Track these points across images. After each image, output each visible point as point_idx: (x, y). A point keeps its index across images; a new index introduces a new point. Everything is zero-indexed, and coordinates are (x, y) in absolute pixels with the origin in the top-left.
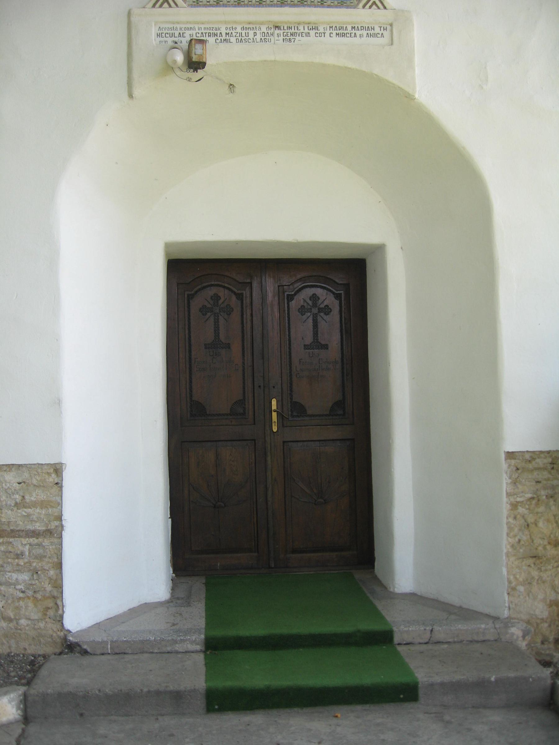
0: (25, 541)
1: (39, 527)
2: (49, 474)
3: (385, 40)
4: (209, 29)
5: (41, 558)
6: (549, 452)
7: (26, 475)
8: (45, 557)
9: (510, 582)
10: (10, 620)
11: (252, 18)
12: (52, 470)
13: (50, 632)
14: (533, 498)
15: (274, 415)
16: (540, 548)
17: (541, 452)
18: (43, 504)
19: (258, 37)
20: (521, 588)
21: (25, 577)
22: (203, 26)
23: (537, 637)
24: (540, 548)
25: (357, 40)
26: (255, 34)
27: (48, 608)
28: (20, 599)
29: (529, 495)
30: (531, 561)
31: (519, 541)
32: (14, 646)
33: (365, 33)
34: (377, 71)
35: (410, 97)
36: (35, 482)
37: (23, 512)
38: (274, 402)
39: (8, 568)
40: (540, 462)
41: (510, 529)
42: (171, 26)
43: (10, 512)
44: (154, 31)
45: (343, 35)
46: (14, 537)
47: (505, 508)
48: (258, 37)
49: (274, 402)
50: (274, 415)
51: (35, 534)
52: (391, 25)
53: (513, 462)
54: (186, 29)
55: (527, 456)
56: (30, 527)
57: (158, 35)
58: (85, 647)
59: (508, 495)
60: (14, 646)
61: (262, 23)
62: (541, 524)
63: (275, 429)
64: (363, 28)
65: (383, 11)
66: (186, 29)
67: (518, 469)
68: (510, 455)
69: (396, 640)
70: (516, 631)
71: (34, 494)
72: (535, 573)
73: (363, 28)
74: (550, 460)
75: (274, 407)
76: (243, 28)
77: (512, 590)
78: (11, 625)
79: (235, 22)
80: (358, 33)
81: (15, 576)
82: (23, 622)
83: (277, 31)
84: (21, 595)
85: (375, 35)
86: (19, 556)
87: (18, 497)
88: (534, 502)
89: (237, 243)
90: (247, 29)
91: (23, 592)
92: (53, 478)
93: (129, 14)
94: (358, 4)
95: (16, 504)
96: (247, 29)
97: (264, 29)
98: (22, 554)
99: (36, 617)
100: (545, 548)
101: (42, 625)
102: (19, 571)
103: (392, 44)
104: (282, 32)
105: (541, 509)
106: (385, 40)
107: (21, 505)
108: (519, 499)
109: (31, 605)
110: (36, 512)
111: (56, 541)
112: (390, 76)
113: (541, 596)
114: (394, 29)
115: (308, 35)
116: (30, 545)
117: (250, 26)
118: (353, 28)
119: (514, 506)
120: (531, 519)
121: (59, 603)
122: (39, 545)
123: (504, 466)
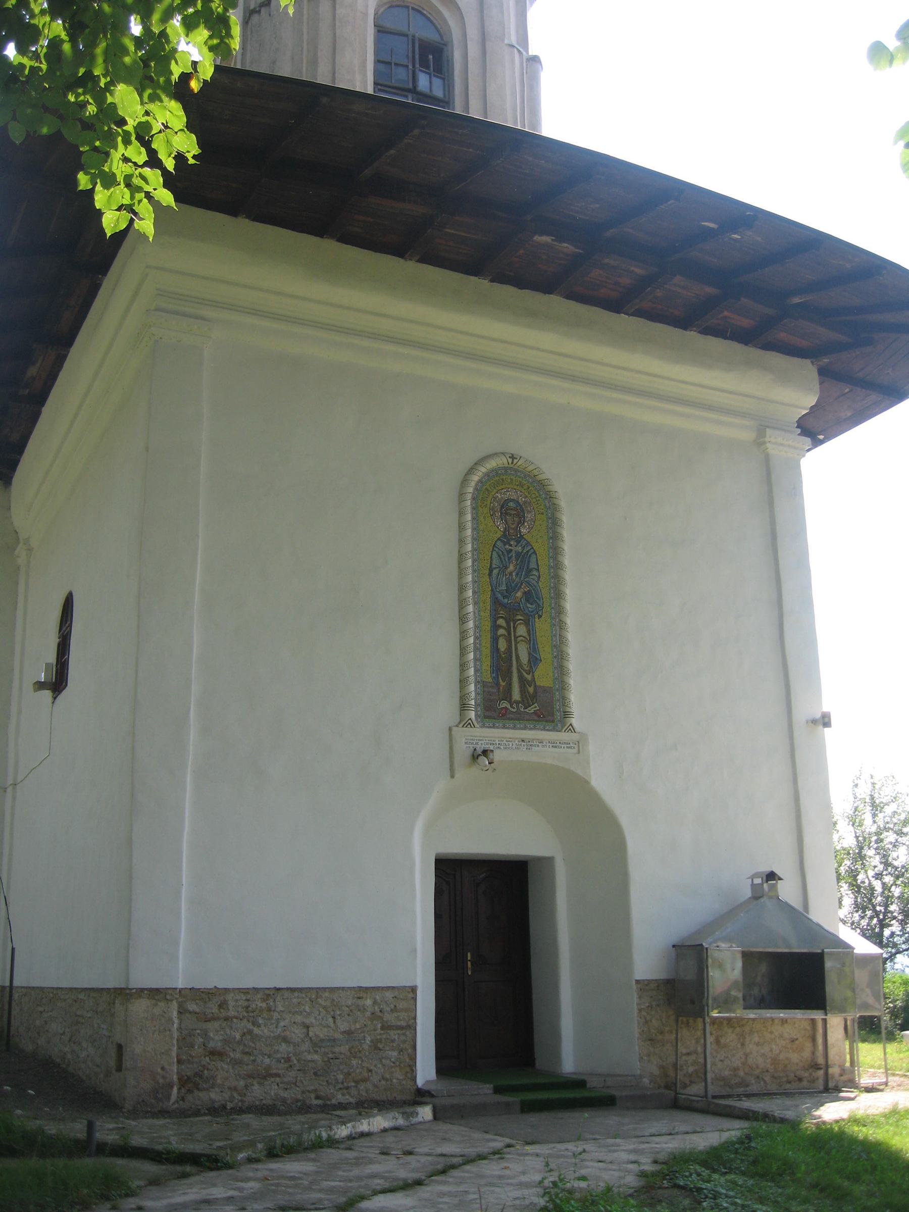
0: (396, 1032)
1: (403, 1023)
2: (409, 992)
3: (575, 751)
4: (490, 740)
5: (404, 1042)
6: (656, 980)
7: (396, 993)
8: (406, 1041)
9: (640, 1054)
10: (387, 1080)
11: (511, 736)
12: (410, 990)
13: (409, 1086)
14: (648, 1006)
15: (469, 963)
16: (654, 1035)
17: (653, 980)
18: (406, 1010)
19: (514, 747)
20: (645, 1058)
21: (395, 1054)
22: (487, 739)
23: (486, 1196)
24: (654, 1035)
25: (562, 750)
26: (513, 745)
27: (407, 1072)
28: (392, 1067)
29: (647, 1005)
30: (649, 1042)
31: (643, 1031)
32: (389, 1095)
33: (565, 746)
34: (572, 768)
35: (587, 782)
36: (401, 997)
37: (395, 1014)
38: (469, 954)
39: (388, 1049)
40: (652, 986)
41: (639, 1023)
42: (472, 738)
43: (388, 1015)
44: (464, 740)
45: (556, 747)
46: (390, 1030)
47: (636, 1011)
48: (514, 747)
49: (469, 954)
50: (469, 963)
51: (401, 1028)
52: (578, 742)
53: (639, 986)
54: (479, 740)
55: (646, 982)
56: (399, 1024)
57: (466, 743)
58: (433, 1093)
59: (638, 1004)
60: (389, 1095)
61: (517, 739)
62: (654, 1021)
63: (470, 973)
64: (565, 743)
65: (574, 734)
66: (479, 740)
67: (641, 990)
68: (638, 982)
69: (588, 1086)
70: (646, 1081)
71: (401, 1004)
72: (652, 1049)
73: (565, 743)
74: (657, 985)
75: (469, 958)
76: (507, 741)
77: (641, 1059)
78: (389, 1083)
79: (503, 738)
80: (563, 746)
81: (390, 1053)
82: (394, 1081)
83: (523, 743)
84: (393, 1065)
85: (570, 747)
86: (393, 1041)
87: (392, 1006)
88: (650, 1008)
89: (456, 854)
90: (509, 741)
91: (394, 1063)
92: (411, 995)
93: (450, 729)
94: (562, 729)
95: (392, 1010)
96: (509, 741)
97: (516, 742)
98: (395, 1040)
99: (401, 1078)
100: (656, 1035)
101: (404, 1082)
102: (393, 1050)
103: (579, 753)
104: (525, 744)
105: (653, 1012)
106: (575, 751)
107: (394, 1010)
108: (642, 1007)
109: (398, 1069)
110: (402, 1015)
111: (413, 1032)
112: (579, 772)
113: (655, 1063)
114: (580, 745)
115: (538, 746)
116: (399, 1034)
117: (511, 740)
118: (560, 743)
119: (640, 1010)
120: (648, 1018)
121: (414, 1069)
122: (404, 1034)
123: (634, 987)
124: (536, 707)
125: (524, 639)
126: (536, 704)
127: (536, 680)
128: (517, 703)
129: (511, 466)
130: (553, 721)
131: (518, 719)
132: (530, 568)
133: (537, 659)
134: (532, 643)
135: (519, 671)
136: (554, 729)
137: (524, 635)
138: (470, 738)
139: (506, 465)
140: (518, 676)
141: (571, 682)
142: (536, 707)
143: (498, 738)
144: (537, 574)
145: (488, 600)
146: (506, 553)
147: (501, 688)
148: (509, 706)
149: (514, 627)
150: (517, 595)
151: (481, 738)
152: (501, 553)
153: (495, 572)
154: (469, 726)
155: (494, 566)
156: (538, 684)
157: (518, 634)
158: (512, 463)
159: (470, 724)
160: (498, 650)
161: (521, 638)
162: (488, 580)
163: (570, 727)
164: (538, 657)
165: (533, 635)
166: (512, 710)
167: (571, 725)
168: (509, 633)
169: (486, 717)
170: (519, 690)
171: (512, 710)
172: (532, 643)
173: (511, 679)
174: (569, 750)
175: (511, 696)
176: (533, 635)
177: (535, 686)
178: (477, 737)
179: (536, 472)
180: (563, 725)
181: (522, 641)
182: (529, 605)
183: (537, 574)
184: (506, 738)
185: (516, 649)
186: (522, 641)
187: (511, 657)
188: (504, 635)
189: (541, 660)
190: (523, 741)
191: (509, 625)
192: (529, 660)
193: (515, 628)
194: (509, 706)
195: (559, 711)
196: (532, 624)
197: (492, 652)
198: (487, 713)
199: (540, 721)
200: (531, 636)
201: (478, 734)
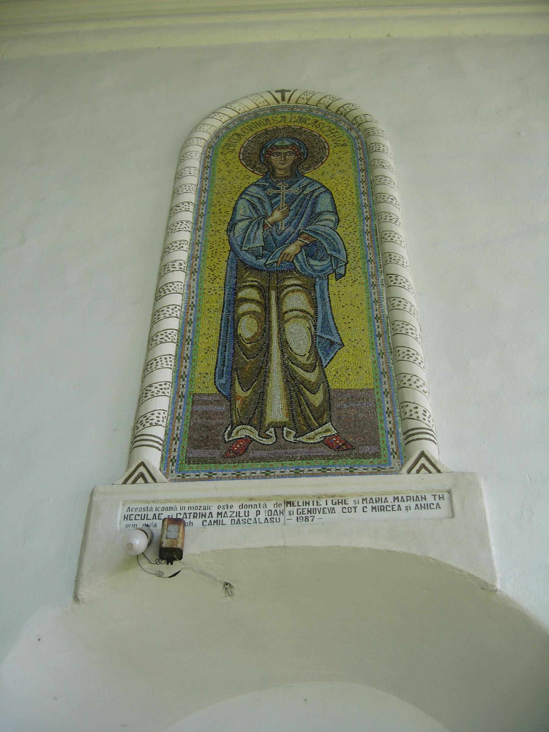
3: (444, 511)
4: (196, 508)
11: (254, 493)
19: (262, 517)
25: (402, 514)
26: (258, 513)
33: (413, 504)
34: (432, 554)
44: (121, 512)
45: (382, 509)
48: (262, 517)
52: (449, 492)
61: (269, 499)
64: (409, 498)
73: (409, 498)
76: (241, 506)
79: (231, 499)
80: (403, 505)
83: (289, 508)
85: (428, 507)
103: (453, 516)
114: (454, 497)
115: (332, 510)
124: (328, 430)
125: (301, 314)
126: (329, 425)
127: (329, 379)
128: (278, 426)
129: (282, 103)
130: (376, 455)
131: (279, 459)
132: (318, 210)
133: (332, 343)
134: (320, 320)
135: (285, 368)
136: (378, 471)
137: (303, 308)
138: (139, 506)
139: (273, 103)
140: (285, 377)
141: (409, 318)
142: (328, 430)
143: (218, 499)
144: (317, 186)
145: (223, 266)
146: (266, 200)
147: (238, 403)
148: (254, 434)
149: (278, 298)
150: (288, 251)
151: (172, 505)
152: (256, 200)
153: (241, 226)
154: (141, 480)
155: (238, 217)
156: (334, 385)
157: (285, 309)
158: (283, 99)
159: (142, 475)
160: (236, 336)
161: (295, 313)
162: (226, 237)
163: (423, 461)
164: (336, 339)
165: (324, 305)
166: (265, 441)
167: (423, 454)
168: (266, 308)
169: (189, 460)
170: (284, 401)
171: (265, 441)
172: (320, 320)
173: (264, 384)
174: (424, 513)
175: (262, 414)
176: (324, 305)
177: (328, 390)
178: (160, 502)
179: (327, 101)
180: (403, 458)
181: (296, 317)
182: (313, 262)
183: (333, 218)
184: (238, 499)
185: (281, 331)
186: (296, 317)
187: (268, 346)
188: (254, 312)
189: (343, 345)
190: (289, 503)
191: (266, 298)
192: (314, 346)
193: (279, 302)
194: (254, 434)
195: (393, 432)
196: (322, 291)
197: (222, 346)
198: (197, 453)
199: (340, 457)
200: (320, 308)
201: (161, 496)
